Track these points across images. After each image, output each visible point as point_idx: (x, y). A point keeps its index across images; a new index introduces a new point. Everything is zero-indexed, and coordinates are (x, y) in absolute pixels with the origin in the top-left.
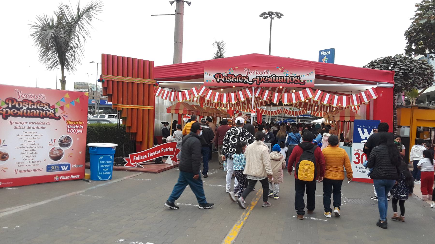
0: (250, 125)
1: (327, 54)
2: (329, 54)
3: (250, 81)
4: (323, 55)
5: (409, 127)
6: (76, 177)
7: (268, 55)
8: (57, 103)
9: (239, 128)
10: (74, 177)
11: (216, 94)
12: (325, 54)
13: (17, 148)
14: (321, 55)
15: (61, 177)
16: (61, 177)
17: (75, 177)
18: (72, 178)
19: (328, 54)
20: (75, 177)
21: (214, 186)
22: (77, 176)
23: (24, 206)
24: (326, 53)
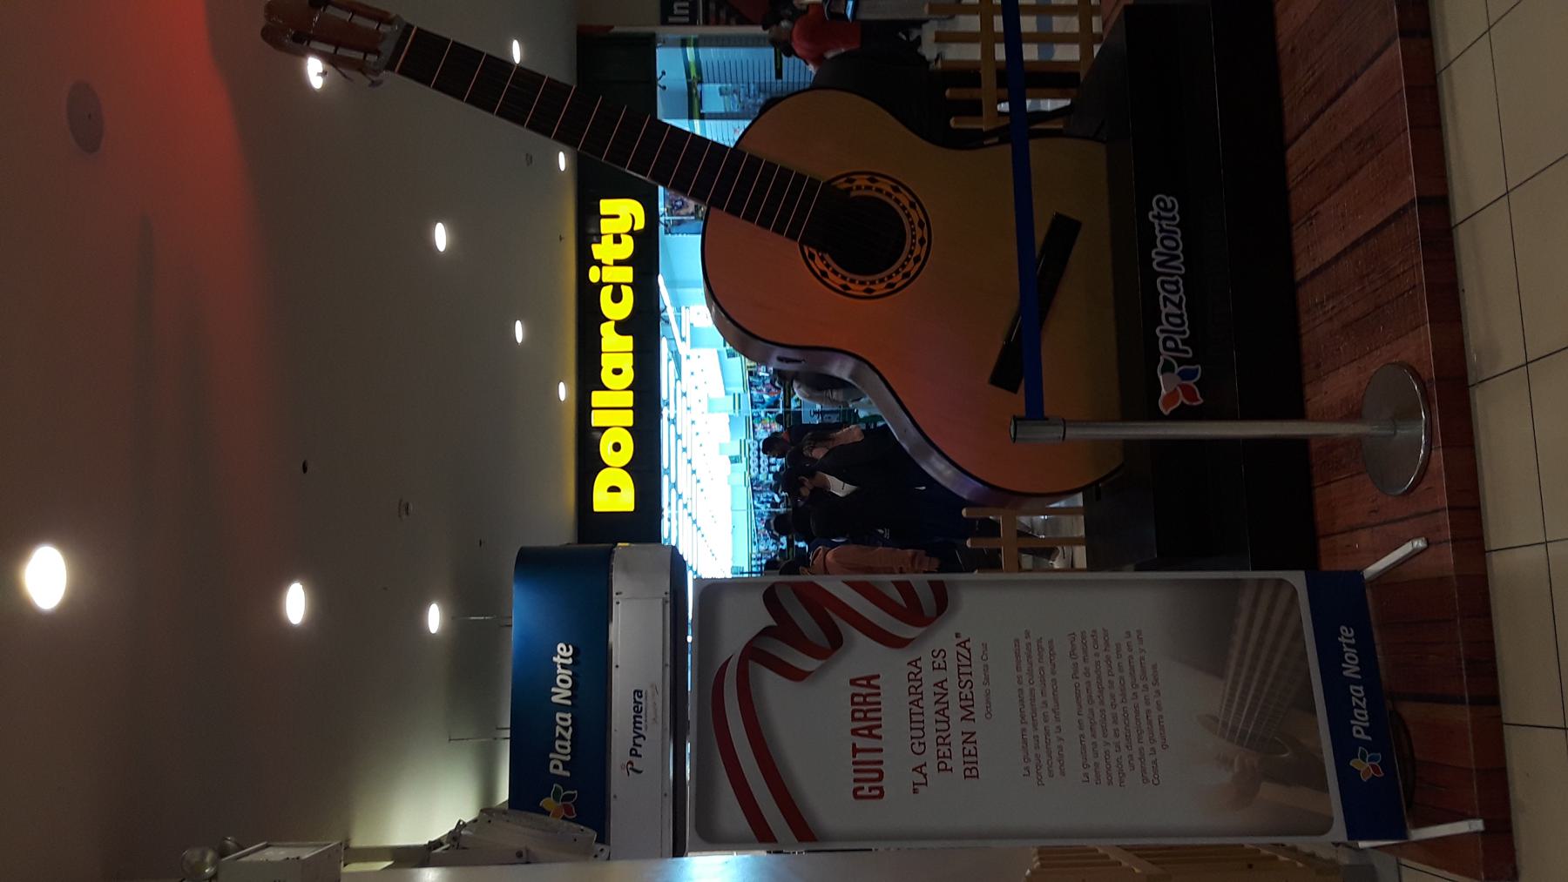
1: (571, 730)
2: (1361, 688)
3: (919, 752)
4: (1367, 724)
5: (1428, 544)
6: (1349, 645)
10: (1353, 659)
11: (1473, 817)
12: (1365, 712)
14: (1370, 738)
15: (1355, 735)
16: (1358, 732)
17: (1350, 653)
18: (569, 693)
19: (1362, 694)
20: (1350, 653)
22: (557, 659)
24: (1358, 707)
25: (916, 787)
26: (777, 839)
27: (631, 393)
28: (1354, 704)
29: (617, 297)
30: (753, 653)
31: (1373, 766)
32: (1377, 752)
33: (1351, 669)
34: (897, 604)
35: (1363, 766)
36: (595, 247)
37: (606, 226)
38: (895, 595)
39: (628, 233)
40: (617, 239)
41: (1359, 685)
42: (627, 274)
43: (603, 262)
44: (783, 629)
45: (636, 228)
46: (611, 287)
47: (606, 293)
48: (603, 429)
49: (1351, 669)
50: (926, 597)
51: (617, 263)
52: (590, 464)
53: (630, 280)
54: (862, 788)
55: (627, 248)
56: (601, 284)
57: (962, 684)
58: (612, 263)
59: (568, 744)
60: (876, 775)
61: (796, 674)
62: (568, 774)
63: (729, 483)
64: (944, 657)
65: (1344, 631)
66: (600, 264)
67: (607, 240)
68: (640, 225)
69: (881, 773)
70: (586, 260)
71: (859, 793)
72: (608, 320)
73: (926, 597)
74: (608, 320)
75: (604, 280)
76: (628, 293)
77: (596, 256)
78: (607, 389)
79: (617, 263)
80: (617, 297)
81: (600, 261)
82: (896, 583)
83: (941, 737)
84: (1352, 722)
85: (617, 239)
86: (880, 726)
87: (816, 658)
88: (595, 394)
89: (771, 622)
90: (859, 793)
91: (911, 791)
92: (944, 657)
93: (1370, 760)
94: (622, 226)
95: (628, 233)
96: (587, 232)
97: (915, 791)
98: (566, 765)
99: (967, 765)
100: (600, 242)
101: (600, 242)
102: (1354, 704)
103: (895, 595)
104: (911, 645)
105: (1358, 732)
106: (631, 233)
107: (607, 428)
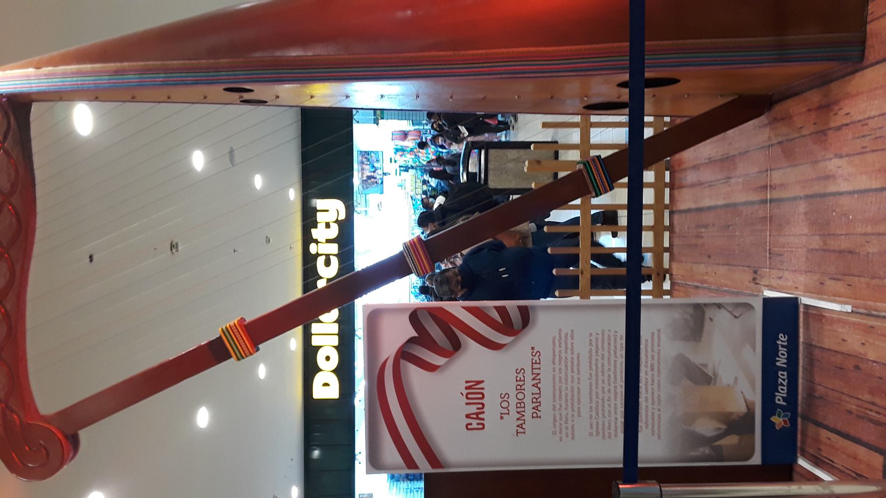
0: (654, 123)
3: (504, 402)
4: (785, 395)
6: (782, 346)
7: (409, 302)
8: (205, 115)
9: (451, 261)
13: (521, 383)
15: (777, 402)
17: (782, 351)
20: (782, 351)
21: (219, 59)
22: (779, 342)
23: (745, 68)
25: (502, 415)
26: (419, 466)
27: (337, 325)
28: (779, 383)
29: (328, 263)
30: (404, 354)
31: (784, 421)
32: (787, 412)
33: (781, 361)
34: (497, 321)
35: (778, 421)
36: (313, 230)
37: (321, 217)
38: (496, 315)
39: (334, 222)
40: (328, 225)
41: (783, 371)
42: (334, 248)
43: (319, 240)
44: (422, 338)
45: (339, 219)
46: (324, 257)
47: (321, 261)
48: (319, 347)
49: (781, 361)
50: (515, 316)
51: (328, 241)
52: (310, 369)
53: (336, 252)
54: (471, 424)
55: (334, 232)
56: (318, 255)
57: (534, 354)
58: (325, 241)
59: (785, 388)
60: (480, 396)
61: (431, 368)
62: (785, 404)
63: (398, 480)
64: (524, 373)
65: (781, 337)
66: (317, 242)
67: (321, 226)
68: (342, 216)
69: (483, 405)
70: (308, 239)
71: (469, 427)
72: (321, 278)
73: (515, 316)
74: (321, 278)
75: (319, 253)
76: (335, 261)
77: (314, 237)
78: (322, 322)
79: (328, 241)
80: (328, 263)
81: (317, 240)
82: (496, 308)
83: (519, 385)
84: (777, 394)
85: (328, 225)
86: (483, 413)
87: (444, 357)
88: (314, 325)
89: (415, 334)
90: (469, 427)
91: (499, 418)
92: (524, 373)
93: (783, 417)
94: (331, 217)
95: (334, 222)
96: (309, 219)
97: (502, 418)
98: (784, 399)
99: (534, 396)
100: (316, 227)
101: (316, 227)
102: (779, 383)
103: (496, 315)
104: (505, 348)
105: (779, 400)
106: (337, 221)
107: (321, 347)
